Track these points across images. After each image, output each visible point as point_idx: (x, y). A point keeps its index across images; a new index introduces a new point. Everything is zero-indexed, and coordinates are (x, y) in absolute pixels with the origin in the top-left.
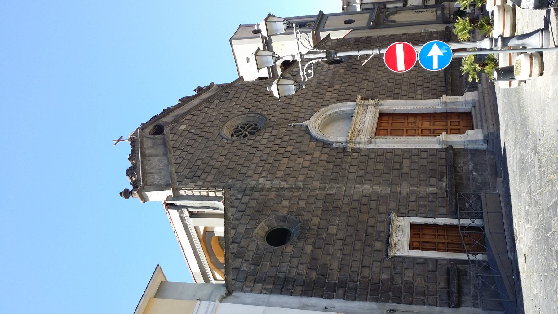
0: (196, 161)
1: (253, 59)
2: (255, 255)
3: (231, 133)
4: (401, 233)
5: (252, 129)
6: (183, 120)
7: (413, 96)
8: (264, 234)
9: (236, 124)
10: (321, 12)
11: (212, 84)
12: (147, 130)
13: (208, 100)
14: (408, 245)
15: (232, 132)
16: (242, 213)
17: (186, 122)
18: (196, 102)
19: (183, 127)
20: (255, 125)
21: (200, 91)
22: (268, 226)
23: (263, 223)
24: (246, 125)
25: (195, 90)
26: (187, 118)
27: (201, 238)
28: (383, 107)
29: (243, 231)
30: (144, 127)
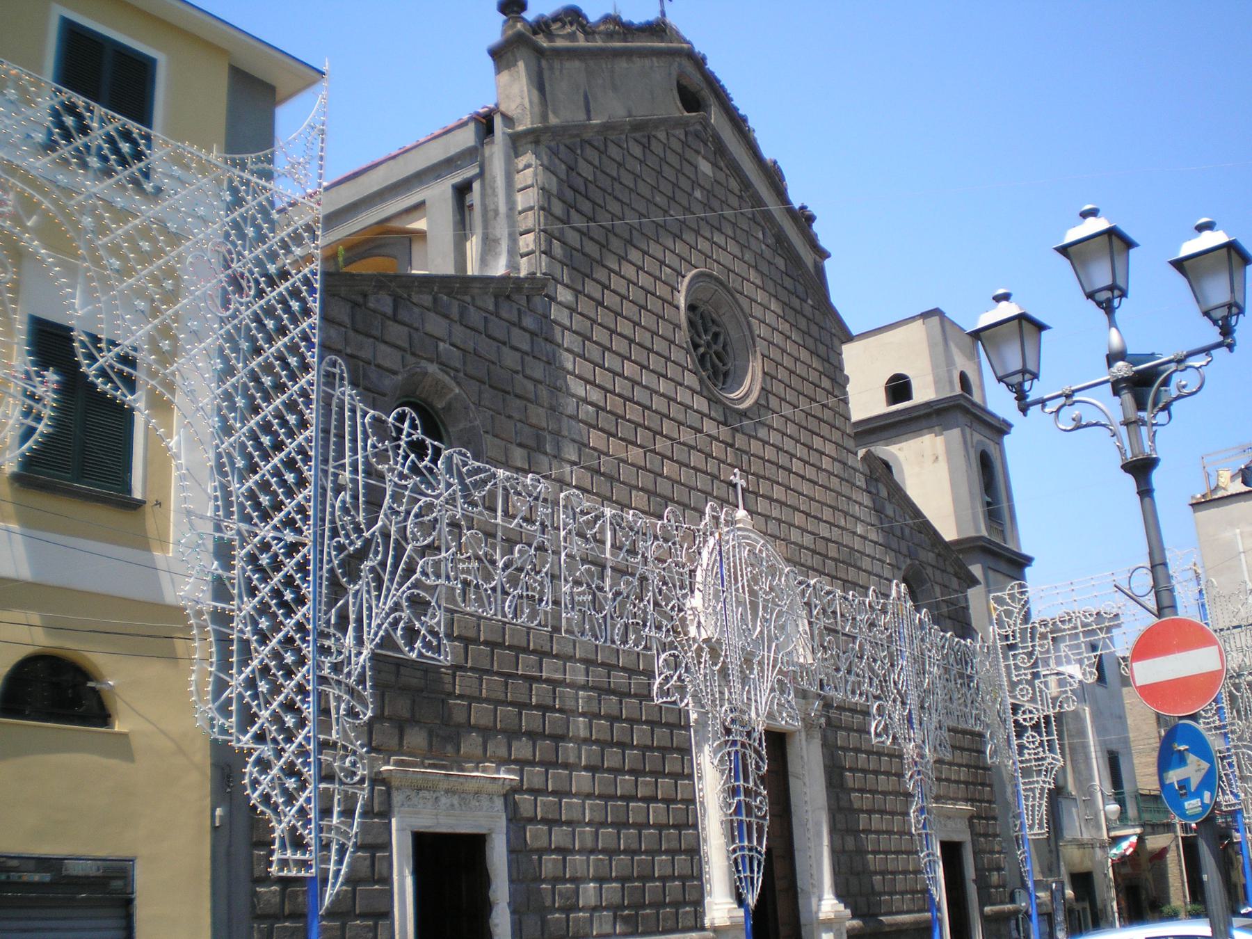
0: (618, 200)
1: (1007, 310)
2: (361, 363)
3: (700, 304)
4: (457, 805)
5: (713, 366)
6: (725, 169)
7: (839, 826)
8: (423, 396)
9: (725, 319)
10: (1028, 561)
11: (824, 254)
12: (689, 68)
13: (781, 240)
14: (426, 827)
15: (702, 308)
16: (482, 328)
17: (721, 177)
18: (774, 207)
19: (705, 167)
20: (726, 375)
21: (804, 219)
22: (448, 408)
23: (457, 390)
24: (724, 347)
25: (803, 208)
26: (732, 180)
27: (395, 224)
28: (804, 742)
29: (429, 328)
30: (699, 62)
